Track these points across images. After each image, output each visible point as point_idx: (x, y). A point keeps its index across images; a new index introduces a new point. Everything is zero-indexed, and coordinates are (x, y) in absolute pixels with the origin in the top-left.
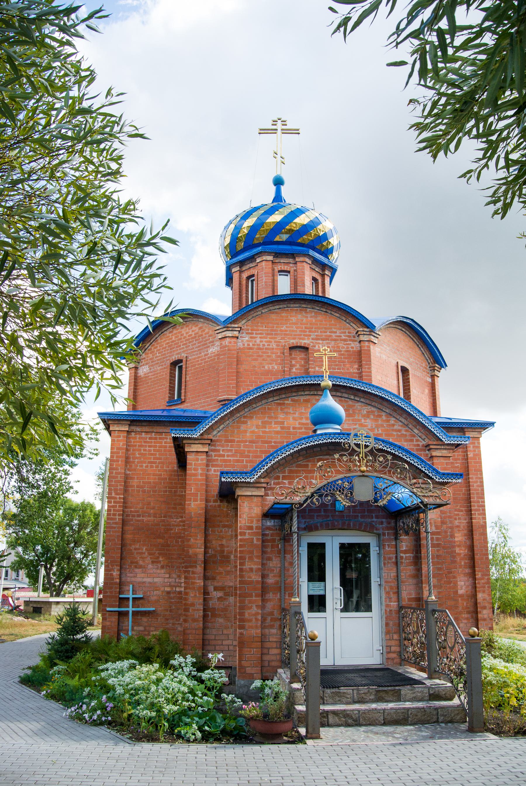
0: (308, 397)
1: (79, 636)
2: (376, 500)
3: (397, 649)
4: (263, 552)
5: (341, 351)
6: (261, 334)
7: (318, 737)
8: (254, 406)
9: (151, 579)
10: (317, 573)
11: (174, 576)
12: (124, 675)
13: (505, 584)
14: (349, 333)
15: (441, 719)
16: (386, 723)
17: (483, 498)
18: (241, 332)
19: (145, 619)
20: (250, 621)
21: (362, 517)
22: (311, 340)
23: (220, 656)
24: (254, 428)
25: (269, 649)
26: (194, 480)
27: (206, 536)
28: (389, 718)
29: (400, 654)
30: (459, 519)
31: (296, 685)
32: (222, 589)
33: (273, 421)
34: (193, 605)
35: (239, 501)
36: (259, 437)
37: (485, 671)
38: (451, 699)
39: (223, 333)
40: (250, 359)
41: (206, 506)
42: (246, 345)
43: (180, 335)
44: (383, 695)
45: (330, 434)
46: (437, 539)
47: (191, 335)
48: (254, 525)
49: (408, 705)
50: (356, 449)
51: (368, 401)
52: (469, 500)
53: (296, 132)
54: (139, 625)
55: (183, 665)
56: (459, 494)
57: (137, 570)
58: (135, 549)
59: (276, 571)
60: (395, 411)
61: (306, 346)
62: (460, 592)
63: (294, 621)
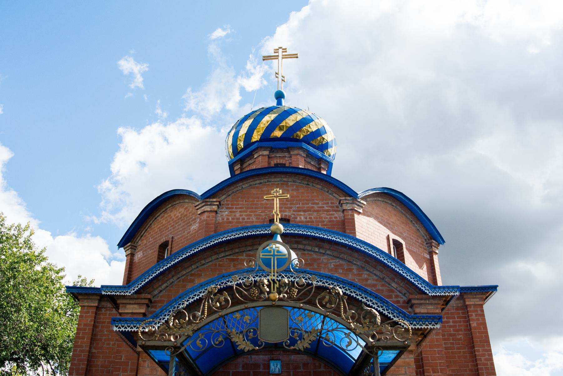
5: (324, 222)
6: (241, 208)
8: (203, 262)
14: (332, 203)
18: (221, 207)
22: (292, 212)
39: (202, 209)
42: (225, 219)
43: (169, 218)
47: (178, 216)
51: (335, 254)
53: (295, 56)
56: (466, 371)
60: (368, 263)
61: (287, 218)
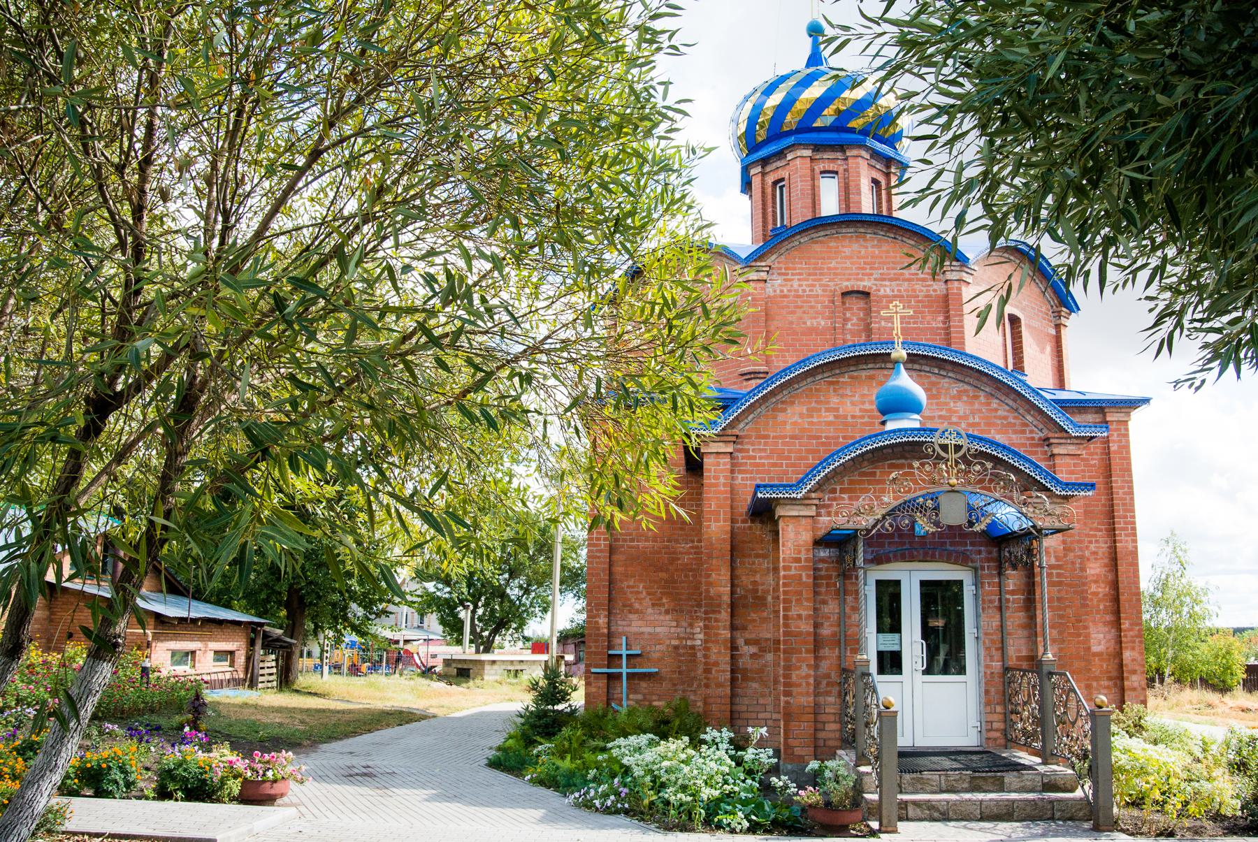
0: (872, 372)
1: (560, 707)
2: (971, 524)
3: (1000, 726)
4: (816, 593)
6: (800, 274)
7: (895, 831)
8: (796, 386)
9: (650, 628)
10: (890, 620)
11: (684, 624)
12: (640, 753)
13: (1180, 636)
15: (1058, 815)
16: (983, 818)
17: (1133, 511)
19: (644, 684)
20: (799, 685)
21: (952, 544)
23: (764, 730)
24: (796, 419)
25: (824, 723)
26: (716, 492)
27: (733, 569)
28: (987, 812)
29: (1005, 733)
30: (1097, 542)
31: (863, 769)
32: (756, 642)
33: (823, 407)
34: (716, 664)
35: (781, 524)
36: (803, 430)
37: (1117, 753)
38: (1072, 791)
40: (784, 311)
41: (732, 528)
44: (981, 783)
45: (906, 430)
46: (1059, 575)
48: (803, 556)
49: (1014, 796)
50: (943, 454)
52: (1111, 514)
54: (636, 692)
55: (718, 740)
57: (631, 616)
58: (628, 587)
59: (834, 618)
60: (999, 389)
62: (1095, 649)
63: (861, 685)
